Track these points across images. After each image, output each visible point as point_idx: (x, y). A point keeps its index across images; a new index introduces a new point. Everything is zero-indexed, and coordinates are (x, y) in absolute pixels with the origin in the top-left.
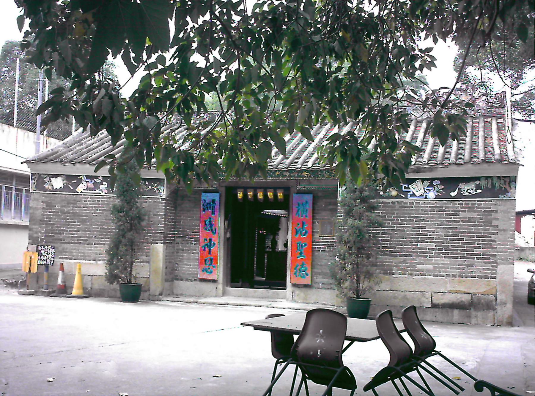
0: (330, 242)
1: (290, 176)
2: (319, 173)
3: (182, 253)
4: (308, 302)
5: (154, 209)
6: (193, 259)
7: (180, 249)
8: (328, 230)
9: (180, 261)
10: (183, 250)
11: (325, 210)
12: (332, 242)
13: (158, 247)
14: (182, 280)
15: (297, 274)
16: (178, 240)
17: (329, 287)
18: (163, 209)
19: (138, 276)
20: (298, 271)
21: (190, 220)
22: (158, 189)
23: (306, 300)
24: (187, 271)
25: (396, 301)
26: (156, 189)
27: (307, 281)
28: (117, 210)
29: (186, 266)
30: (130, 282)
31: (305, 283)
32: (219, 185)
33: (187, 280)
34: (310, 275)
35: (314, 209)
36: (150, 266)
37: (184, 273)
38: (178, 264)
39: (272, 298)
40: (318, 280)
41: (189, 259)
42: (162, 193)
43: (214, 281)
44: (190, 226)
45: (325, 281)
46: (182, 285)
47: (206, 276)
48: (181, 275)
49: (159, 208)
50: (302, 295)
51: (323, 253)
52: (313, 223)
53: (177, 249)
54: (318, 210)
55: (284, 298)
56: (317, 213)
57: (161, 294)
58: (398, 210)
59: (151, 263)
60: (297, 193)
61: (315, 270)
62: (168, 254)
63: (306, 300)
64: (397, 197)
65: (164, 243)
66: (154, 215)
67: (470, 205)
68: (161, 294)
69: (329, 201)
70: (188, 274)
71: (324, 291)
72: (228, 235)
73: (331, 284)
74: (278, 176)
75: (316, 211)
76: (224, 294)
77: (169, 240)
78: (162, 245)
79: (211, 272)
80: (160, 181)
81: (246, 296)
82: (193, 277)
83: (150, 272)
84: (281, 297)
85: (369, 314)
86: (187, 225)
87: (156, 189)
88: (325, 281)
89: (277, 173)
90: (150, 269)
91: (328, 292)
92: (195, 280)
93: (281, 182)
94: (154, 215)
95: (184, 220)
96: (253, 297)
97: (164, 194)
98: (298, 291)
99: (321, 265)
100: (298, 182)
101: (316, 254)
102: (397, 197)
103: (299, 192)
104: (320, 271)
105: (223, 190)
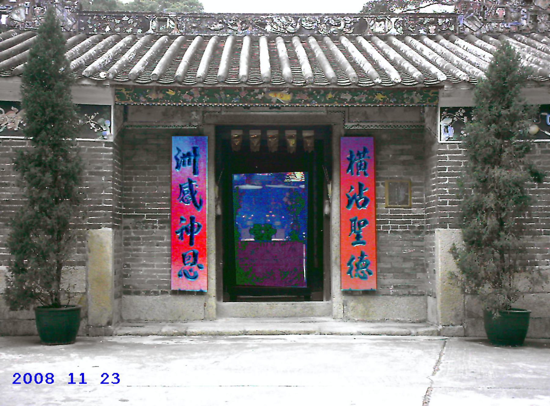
0: (405, 217)
1: (353, 101)
2: (405, 96)
3: (135, 244)
4: (370, 318)
5: (91, 162)
6: (157, 255)
7: (133, 238)
8: (402, 197)
9: (132, 260)
10: (139, 239)
11: (393, 163)
12: (408, 217)
13: (101, 235)
14: (138, 293)
15: (353, 272)
16: (127, 221)
17: (407, 292)
18: (109, 162)
19: (72, 290)
20: (354, 268)
21: (149, 184)
22: (97, 126)
23: (368, 316)
24: (148, 276)
25: (542, 309)
26: (93, 125)
27: (370, 284)
28: (22, 162)
29: (144, 269)
30: (57, 304)
31: (368, 287)
32: (203, 121)
33: (148, 293)
34: (374, 272)
35: (376, 163)
36: (87, 269)
37: (142, 282)
38: (128, 266)
39: (302, 316)
40: (386, 282)
41: (150, 256)
42: (108, 133)
43: (201, 293)
44: (149, 195)
45: (399, 282)
46: (141, 303)
47: (185, 284)
48: (136, 285)
49: (102, 162)
50: (361, 308)
51: (393, 236)
52: (376, 185)
53: (126, 239)
54: (381, 163)
55: (329, 313)
56: (380, 169)
57: (109, 323)
58: (540, 157)
59: (89, 264)
60: (346, 135)
61: (381, 265)
62: (466, 238)
63: (368, 316)
64: (539, 135)
65: (113, 227)
66: (91, 173)
67: (447, 171)
68: (109, 323)
69: (399, 147)
70: (150, 282)
71: (397, 300)
72: (219, 212)
73: (409, 287)
74: (331, 101)
75: (379, 165)
76: (219, 313)
77: (117, 223)
78: (110, 229)
79: (195, 277)
80: (101, 110)
81: (256, 316)
82: (159, 287)
83: (87, 282)
84: (318, 314)
85: (528, 335)
86: (143, 195)
87: (93, 125)
88: (399, 282)
89: (330, 96)
90: (87, 276)
91: (404, 300)
92: (163, 293)
93: (317, 116)
94: (91, 173)
95: (138, 184)
96: (268, 316)
97: (110, 135)
98: (352, 302)
99: (391, 256)
100: (346, 114)
101: (382, 237)
102: (539, 135)
103: (349, 134)
104: (389, 266)
105: (210, 130)
